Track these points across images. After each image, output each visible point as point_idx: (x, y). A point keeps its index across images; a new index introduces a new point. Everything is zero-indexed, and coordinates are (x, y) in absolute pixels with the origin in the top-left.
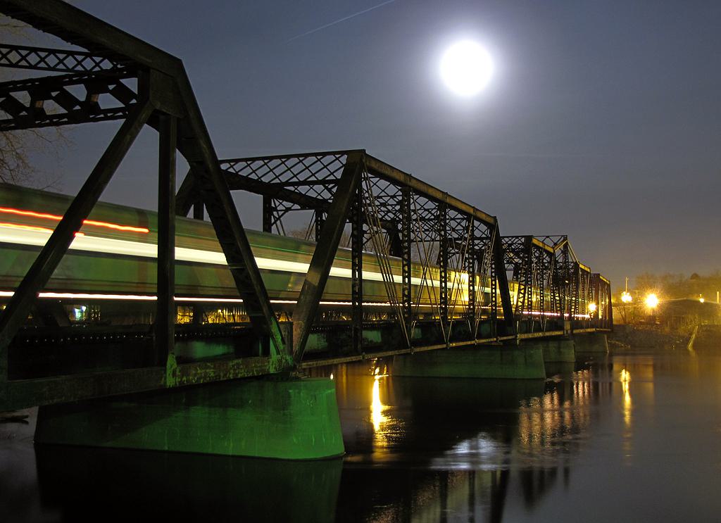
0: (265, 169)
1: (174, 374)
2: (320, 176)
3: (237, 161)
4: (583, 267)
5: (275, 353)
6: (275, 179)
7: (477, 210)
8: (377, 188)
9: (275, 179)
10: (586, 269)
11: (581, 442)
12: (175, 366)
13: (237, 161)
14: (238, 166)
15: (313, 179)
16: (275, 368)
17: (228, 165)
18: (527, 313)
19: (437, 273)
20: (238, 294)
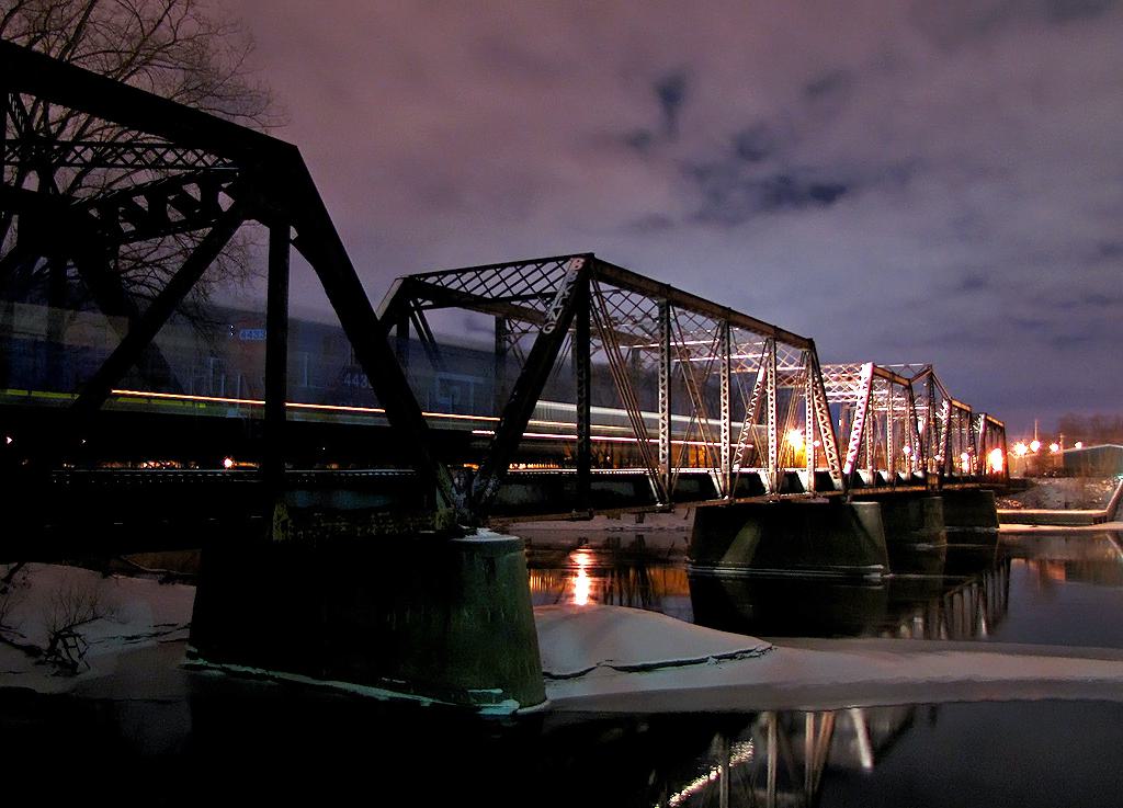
0: (477, 281)
1: (284, 526)
2: (537, 288)
3: (464, 271)
4: (958, 404)
5: (444, 504)
6: (526, 289)
7: (781, 330)
8: (621, 305)
9: (526, 289)
10: (964, 407)
11: (743, 775)
12: (285, 517)
13: (445, 273)
14: (445, 281)
15: (529, 292)
16: (444, 524)
17: (435, 279)
18: (465, 556)
19: (600, 433)
20: (428, 421)
